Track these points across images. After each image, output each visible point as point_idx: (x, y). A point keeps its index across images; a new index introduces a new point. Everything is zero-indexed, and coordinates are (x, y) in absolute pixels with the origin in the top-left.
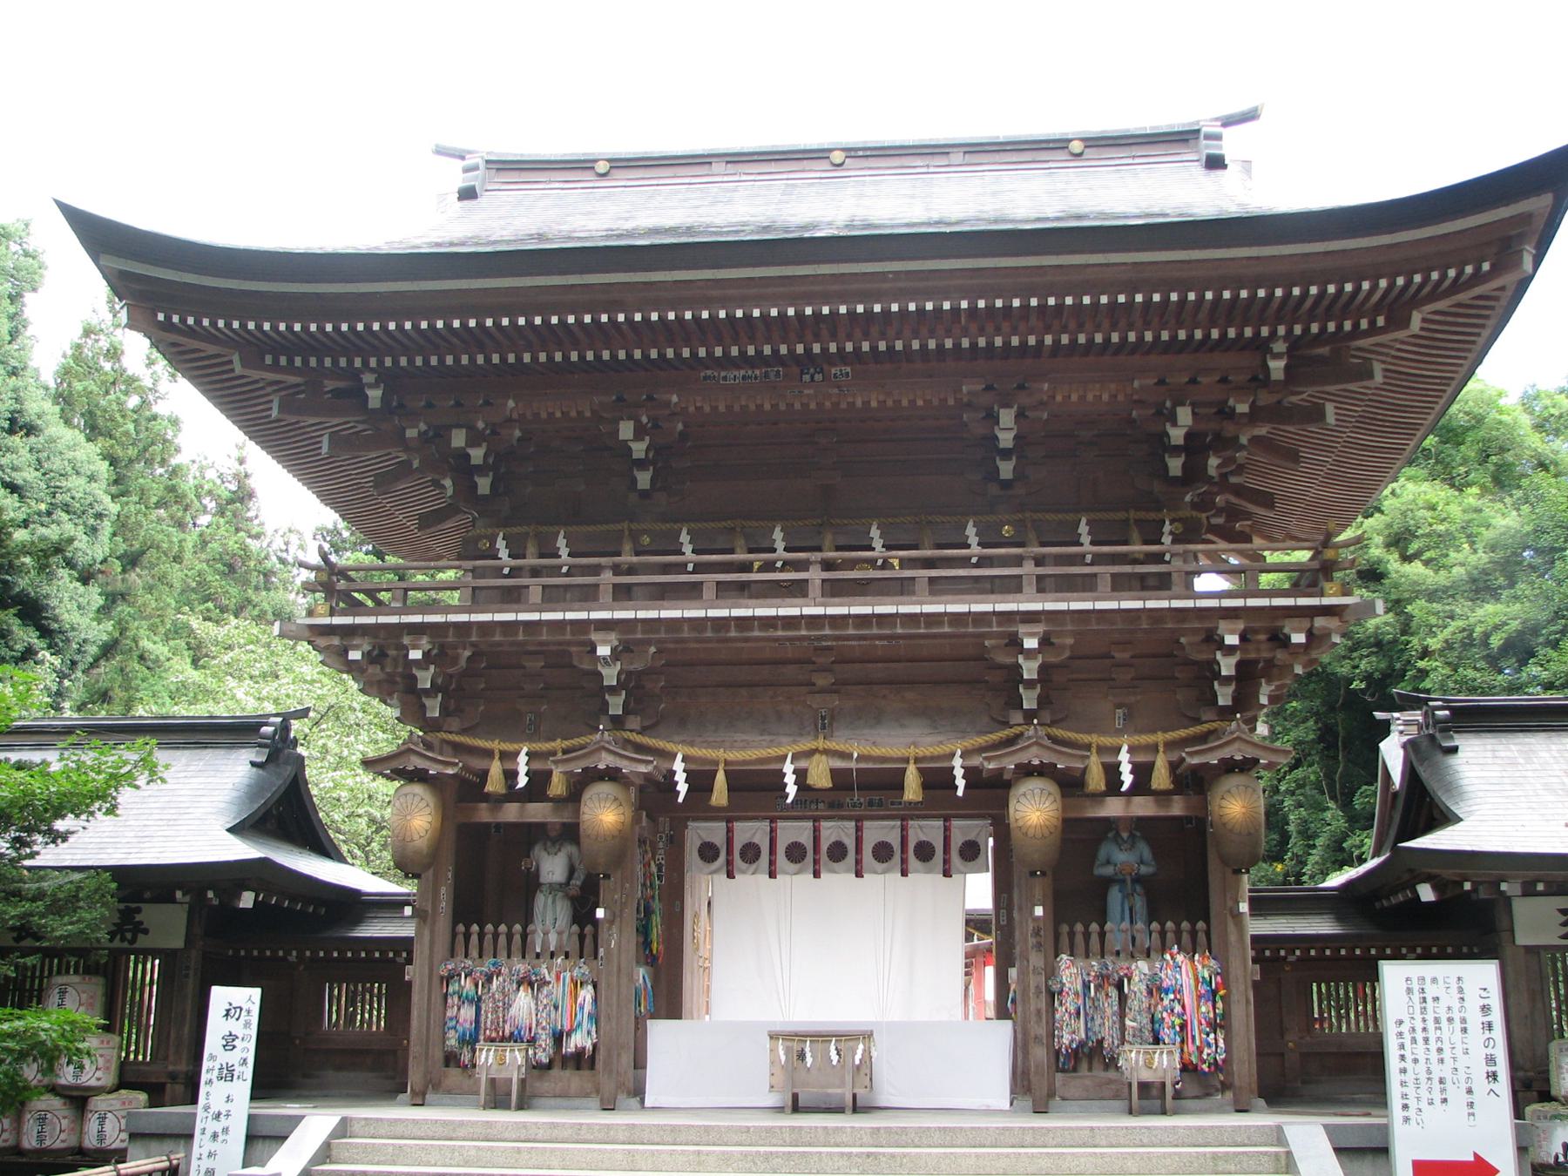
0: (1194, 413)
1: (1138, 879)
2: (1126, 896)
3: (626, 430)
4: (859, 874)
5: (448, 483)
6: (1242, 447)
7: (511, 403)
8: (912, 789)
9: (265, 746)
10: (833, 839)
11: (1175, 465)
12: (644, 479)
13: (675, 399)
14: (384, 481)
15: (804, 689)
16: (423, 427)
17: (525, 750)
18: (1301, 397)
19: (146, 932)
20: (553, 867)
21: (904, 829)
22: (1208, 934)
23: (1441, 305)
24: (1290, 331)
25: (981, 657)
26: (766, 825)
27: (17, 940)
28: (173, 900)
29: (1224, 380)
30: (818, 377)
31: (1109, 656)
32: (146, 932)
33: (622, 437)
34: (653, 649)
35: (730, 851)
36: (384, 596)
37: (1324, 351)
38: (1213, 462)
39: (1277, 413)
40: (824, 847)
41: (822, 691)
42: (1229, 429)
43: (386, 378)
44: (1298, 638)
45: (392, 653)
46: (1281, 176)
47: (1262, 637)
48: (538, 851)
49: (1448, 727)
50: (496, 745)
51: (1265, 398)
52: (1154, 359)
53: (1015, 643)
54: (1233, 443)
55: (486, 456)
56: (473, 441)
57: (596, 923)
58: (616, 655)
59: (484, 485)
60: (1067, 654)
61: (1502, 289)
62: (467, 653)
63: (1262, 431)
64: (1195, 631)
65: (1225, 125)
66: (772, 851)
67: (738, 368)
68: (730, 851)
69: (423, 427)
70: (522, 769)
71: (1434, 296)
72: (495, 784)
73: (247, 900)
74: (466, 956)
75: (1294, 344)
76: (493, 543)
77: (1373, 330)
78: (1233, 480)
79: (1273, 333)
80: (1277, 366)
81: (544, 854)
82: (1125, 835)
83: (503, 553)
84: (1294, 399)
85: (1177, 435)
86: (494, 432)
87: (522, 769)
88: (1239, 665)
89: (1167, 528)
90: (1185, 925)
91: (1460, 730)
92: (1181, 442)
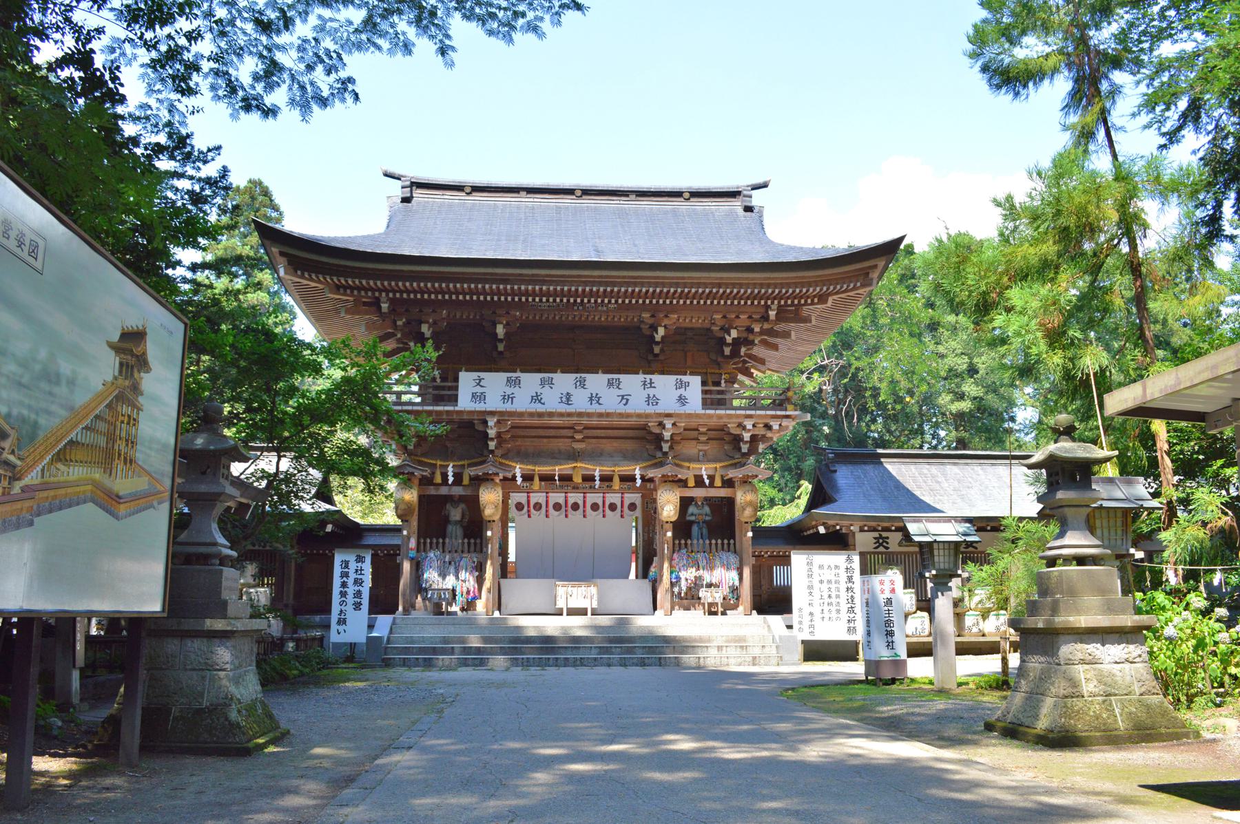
2: (700, 529)
11: (727, 351)
18: (780, 327)
20: (456, 514)
29: (750, 317)
33: (1018, 655)
39: (771, 333)
41: (578, 441)
42: (751, 337)
43: (392, 302)
44: (776, 427)
48: (448, 506)
49: (834, 461)
51: (766, 326)
54: (752, 343)
70: (450, 474)
71: (837, 293)
73: (329, 528)
80: (772, 314)
87: (450, 474)
90: (435, 541)
91: (837, 462)
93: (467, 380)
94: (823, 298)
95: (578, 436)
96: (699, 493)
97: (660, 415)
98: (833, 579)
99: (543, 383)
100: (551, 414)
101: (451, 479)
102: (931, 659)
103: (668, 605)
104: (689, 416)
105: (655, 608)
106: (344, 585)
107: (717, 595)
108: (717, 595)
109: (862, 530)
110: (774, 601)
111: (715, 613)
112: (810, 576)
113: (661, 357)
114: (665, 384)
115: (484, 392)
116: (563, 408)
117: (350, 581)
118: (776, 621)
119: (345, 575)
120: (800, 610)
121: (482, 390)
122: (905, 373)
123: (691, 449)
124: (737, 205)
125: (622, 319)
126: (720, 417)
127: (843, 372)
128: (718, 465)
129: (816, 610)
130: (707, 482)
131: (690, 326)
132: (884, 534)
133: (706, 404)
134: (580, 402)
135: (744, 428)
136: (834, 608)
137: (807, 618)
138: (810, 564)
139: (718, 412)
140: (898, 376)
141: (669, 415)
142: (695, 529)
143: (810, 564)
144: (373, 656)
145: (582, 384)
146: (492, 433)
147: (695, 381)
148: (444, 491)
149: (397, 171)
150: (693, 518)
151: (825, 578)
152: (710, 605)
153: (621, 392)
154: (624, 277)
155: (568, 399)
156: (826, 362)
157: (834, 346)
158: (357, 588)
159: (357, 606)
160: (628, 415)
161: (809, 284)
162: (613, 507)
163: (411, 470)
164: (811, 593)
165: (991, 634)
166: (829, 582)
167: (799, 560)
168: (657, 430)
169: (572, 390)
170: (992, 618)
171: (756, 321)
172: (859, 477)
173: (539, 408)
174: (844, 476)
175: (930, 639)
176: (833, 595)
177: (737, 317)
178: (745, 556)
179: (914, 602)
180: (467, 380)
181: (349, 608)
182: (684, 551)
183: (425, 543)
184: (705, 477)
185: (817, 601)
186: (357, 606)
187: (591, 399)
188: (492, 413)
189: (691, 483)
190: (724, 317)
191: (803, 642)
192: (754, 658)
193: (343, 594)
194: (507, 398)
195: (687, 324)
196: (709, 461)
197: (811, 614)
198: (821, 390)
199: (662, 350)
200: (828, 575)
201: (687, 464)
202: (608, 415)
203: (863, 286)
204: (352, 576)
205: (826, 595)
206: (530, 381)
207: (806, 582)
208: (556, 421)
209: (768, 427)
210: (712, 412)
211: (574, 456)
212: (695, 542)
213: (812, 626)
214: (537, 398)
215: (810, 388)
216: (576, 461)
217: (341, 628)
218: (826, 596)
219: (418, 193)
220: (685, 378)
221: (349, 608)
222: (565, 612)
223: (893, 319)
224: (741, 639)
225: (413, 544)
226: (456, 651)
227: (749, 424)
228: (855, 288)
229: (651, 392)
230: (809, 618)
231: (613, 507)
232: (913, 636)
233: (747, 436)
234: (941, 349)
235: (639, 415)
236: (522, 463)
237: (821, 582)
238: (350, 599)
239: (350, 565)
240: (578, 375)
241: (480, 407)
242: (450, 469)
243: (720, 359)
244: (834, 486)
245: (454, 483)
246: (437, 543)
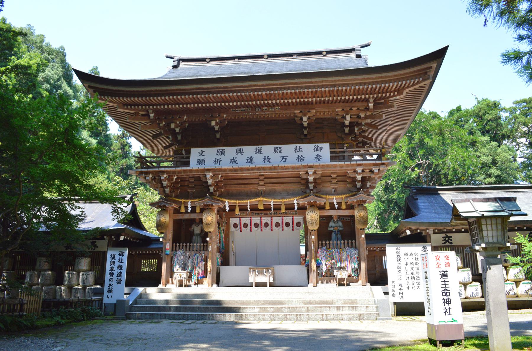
0: (351, 117)
1: (339, 231)
3: (213, 123)
5: (170, 137)
6: (363, 125)
7: (185, 117)
12: (218, 136)
13: (225, 116)
14: (155, 137)
15: (257, 185)
16: (164, 123)
17: (190, 201)
19: (97, 247)
21: (240, 220)
22: (355, 243)
23: (411, 89)
24: (373, 97)
25: (299, 177)
27: (66, 249)
28: (103, 239)
29: (358, 109)
30: (260, 110)
31: (330, 176)
32: (97, 247)
34: (220, 176)
35: (240, 225)
36: (154, 164)
37: (382, 101)
38: (356, 129)
39: (371, 117)
40: (263, 224)
42: (360, 121)
43: (156, 112)
44: (376, 171)
45: (157, 178)
46: (375, 59)
47: (368, 171)
48: (193, 226)
50: (183, 201)
51: (368, 113)
52: (341, 104)
53: (307, 173)
55: (180, 130)
56: (177, 126)
57: (207, 242)
58: (212, 177)
59: (179, 138)
60: (320, 175)
61: (426, 85)
62: (175, 177)
63: (368, 121)
64: (351, 170)
65: (361, 47)
66: (251, 225)
67: (240, 108)
68: (240, 225)
69: (164, 123)
70: (189, 206)
71: (408, 87)
72: (183, 210)
73: (122, 238)
75: (375, 100)
76: (182, 151)
77: (394, 96)
78: (363, 134)
79: (369, 97)
80: (371, 105)
82: (336, 220)
83: (184, 153)
84: (375, 113)
85: (347, 123)
86: (182, 125)
87: (189, 206)
88: (362, 178)
89: (345, 145)
90: (350, 241)
92: (348, 124)
93: (195, 153)
94: (399, 91)
95: (262, 183)
97: (305, 167)
98: (414, 262)
99: (237, 152)
100: (242, 169)
101: (190, 210)
102: (484, 312)
103: (315, 280)
104: (323, 166)
105: (309, 283)
106: (112, 269)
107: (344, 274)
108: (344, 274)
109: (434, 233)
110: (378, 278)
111: (344, 285)
112: (399, 260)
113: (309, 137)
114: (308, 150)
115: (205, 159)
116: (248, 166)
117: (116, 267)
118: (378, 289)
119: (113, 263)
120: (393, 282)
121: (203, 158)
122: (460, 166)
123: (329, 187)
124: (353, 55)
125: (284, 114)
126: (341, 166)
127: (430, 166)
128: (343, 196)
129: (404, 282)
130: (336, 206)
131: (323, 117)
132: (449, 235)
133: (333, 159)
134: (258, 161)
135: (357, 173)
136: (415, 281)
137: (397, 288)
138: (398, 252)
139: (340, 163)
140: (457, 167)
141: (311, 167)
142: (333, 235)
143: (398, 252)
144: (121, 312)
145: (259, 151)
146: (210, 182)
147: (326, 147)
148: (187, 216)
149: (172, 55)
150: (332, 229)
151: (409, 261)
152: (340, 280)
153: (282, 155)
154: (276, 85)
155: (251, 160)
156: (421, 162)
157: (424, 155)
158: (119, 271)
159: (119, 282)
160: (287, 168)
161: (390, 81)
162: (287, 225)
163: (164, 204)
164: (400, 271)
165: (522, 296)
166: (412, 263)
167: (391, 250)
168: (305, 177)
169: (254, 155)
170: (521, 285)
171: (362, 110)
172: (432, 202)
173: (235, 166)
174: (422, 202)
175: (483, 300)
176: (415, 272)
177: (351, 109)
178: (361, 250)
179: (471, 276)
180: (195, 153)
181: (114, 283)
182: (325, 248)
183: (176, 246)
184: (335, 203)
185: (404, 276)
186: (119, 282)
187: (265, 159)
188: (209, 170)
189: (328, 207)
190: (343, 110)
191: (395, 303)
192: (360, 315)
193: (111, 274)
194: (217, 161)
195: (322, 116)
196: (338, 194)
197: (400, 285)
198: (420, 176)
199: (309, 133)
200: (411, 259)
201: (324, 196)
202: (275, 168)
203: (424, 80)
204: (117, 263)
205: (409, 272)
206: (230, 151)
207: (396, 264)
208: (246, 174)
209: (372, 171)
210: (336, 163)
211: (258, 194)
212: (335, 242)
213: (401, 293)
214: (234, 161)
215: (414, 175)
216: (260, 197)
217: (109, 295)
218: (410, 273)
219: (182, 64)
220: (320, 145)
221: (114, 283)
222: (254, 285)
223: (453, 141)
224: (354, 302)
225: (168, 246)
226: (172, 309)
227: (359, 170)
228: (419, 82)
229: (300, 154)
230: (399, 287)
231: (287, 225)
232: (471, 298)
233: (359, 177)
234: (478, 153)
235: (293, 168)
236: (229, 199)
237: (406, 264)
238: (115, 277)
240: (257, 147)
241: (201, 167)
242: (189, 204)
243: (343, 136)
244: (417, 208)
245: (191, 212)
246: (183, 246)
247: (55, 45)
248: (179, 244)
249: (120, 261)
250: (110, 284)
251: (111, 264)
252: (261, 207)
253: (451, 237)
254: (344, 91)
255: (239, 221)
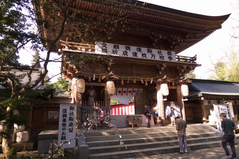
4: (117, 95)
8: (122, 83)
9: (40, 73)
10: (129, 90)
21: (122, 89)
26: (122, 88)
74: (102, 106)
81: (91, 91)
96: (91, 84)
101: (94, 79)
106: (64, 120)
117: (67, 119)
158: (70, 122)
239: (67, 111)
247: (223, 25)
248: (172, 102)
249: (71, 114)
250: (63, 133)
251: (63, 117)
252: (135, 81)
253: (210, 101)
254: (96, 6)
255: (132, 90)
